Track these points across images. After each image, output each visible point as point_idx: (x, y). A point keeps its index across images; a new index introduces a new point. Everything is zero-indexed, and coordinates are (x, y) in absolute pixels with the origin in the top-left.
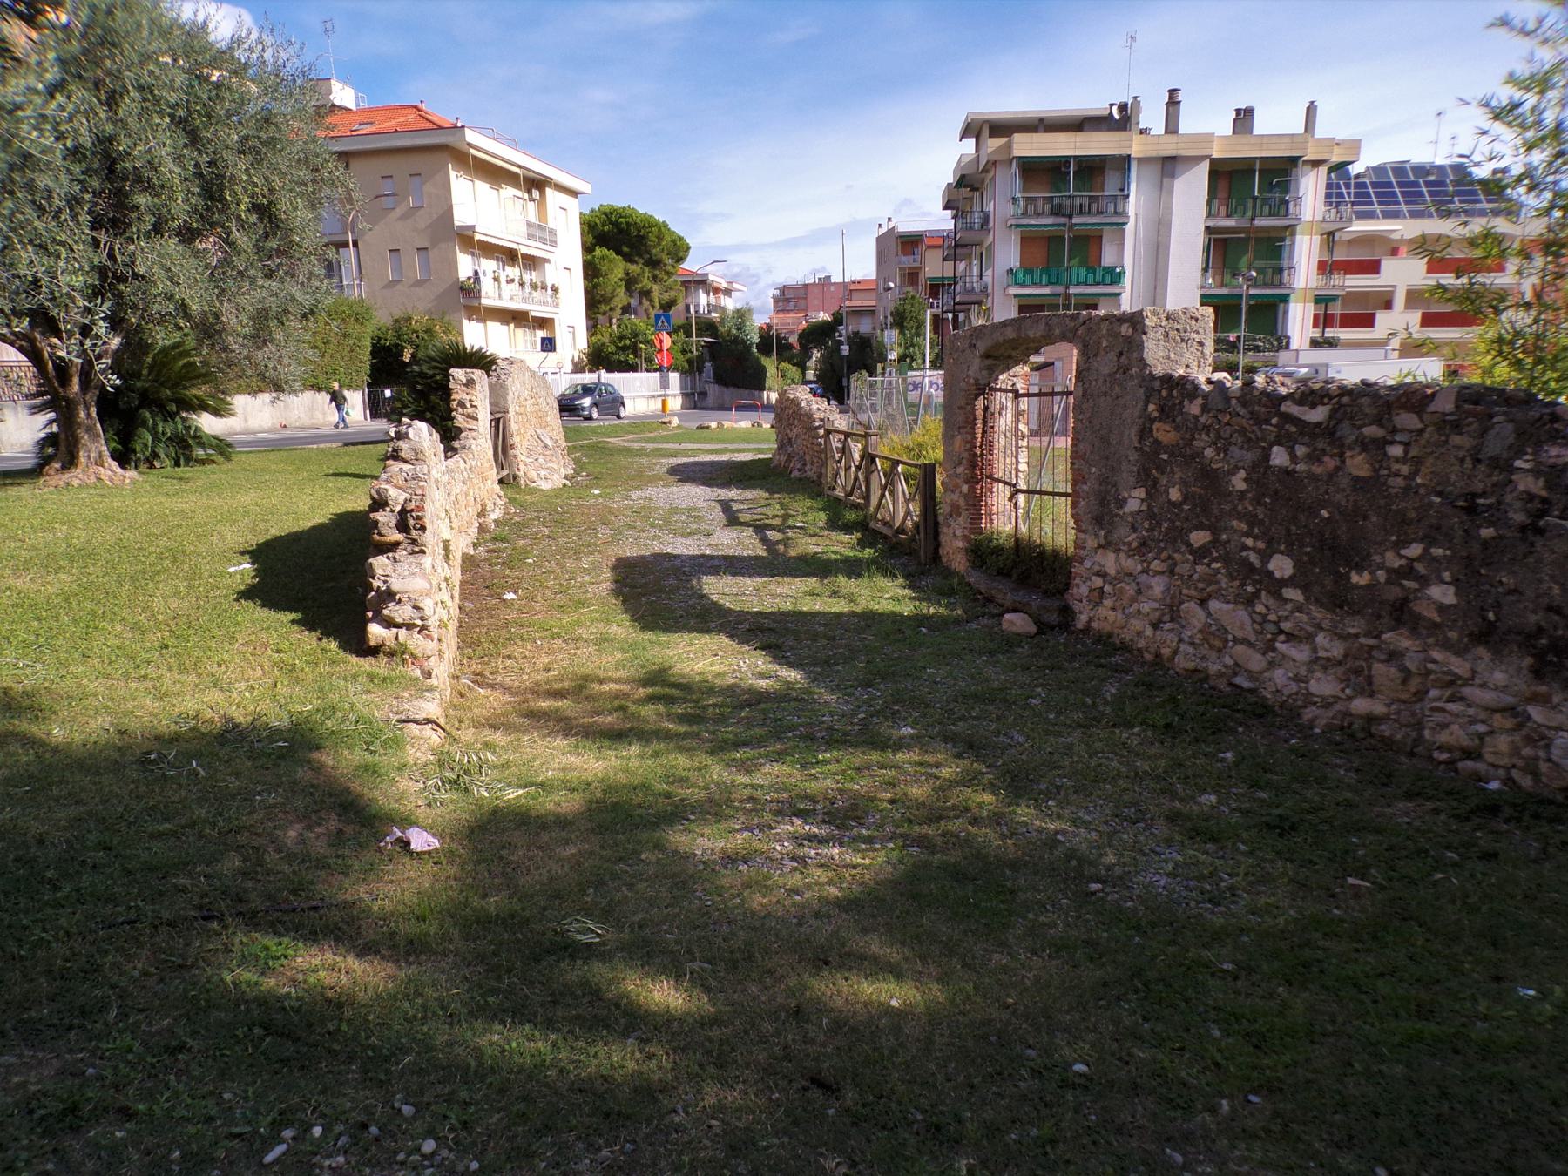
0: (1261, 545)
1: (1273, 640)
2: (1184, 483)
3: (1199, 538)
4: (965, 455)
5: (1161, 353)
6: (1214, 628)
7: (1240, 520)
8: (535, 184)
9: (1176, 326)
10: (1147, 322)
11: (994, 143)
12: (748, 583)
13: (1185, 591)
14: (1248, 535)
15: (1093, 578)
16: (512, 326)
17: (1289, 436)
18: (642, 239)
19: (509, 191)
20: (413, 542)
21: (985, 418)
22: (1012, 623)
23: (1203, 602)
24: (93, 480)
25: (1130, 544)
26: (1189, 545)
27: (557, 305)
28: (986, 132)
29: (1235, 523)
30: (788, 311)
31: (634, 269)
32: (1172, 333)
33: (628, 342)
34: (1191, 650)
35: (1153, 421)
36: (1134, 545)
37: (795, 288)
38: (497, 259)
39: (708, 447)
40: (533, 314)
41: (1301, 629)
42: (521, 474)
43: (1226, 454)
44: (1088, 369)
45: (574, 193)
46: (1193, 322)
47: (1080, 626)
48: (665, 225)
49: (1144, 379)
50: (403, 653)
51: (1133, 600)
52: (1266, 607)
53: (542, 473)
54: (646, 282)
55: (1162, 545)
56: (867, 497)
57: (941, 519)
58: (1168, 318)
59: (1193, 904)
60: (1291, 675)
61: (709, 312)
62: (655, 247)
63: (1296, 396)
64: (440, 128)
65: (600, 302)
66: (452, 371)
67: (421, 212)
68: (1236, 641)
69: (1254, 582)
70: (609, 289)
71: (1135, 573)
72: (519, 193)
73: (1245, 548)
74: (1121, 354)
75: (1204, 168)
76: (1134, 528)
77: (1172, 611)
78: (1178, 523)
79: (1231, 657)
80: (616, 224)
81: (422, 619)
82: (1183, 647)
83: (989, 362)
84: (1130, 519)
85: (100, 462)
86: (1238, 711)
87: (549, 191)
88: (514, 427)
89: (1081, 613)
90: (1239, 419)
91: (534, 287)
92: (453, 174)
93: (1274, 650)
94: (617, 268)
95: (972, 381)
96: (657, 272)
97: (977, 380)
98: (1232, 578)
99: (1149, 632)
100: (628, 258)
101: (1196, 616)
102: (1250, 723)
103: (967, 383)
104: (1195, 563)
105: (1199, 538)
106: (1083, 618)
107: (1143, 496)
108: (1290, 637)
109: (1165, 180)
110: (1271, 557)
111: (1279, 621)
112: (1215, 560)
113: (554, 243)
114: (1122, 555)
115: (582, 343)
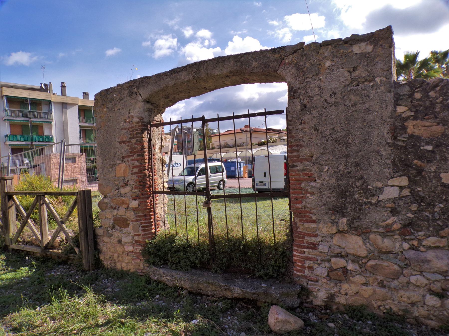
83: (149, 106)
84: (390, 205)
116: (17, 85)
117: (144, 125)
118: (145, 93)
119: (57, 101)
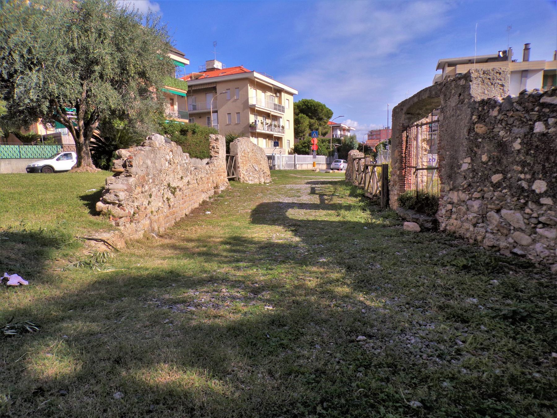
0: (528, 176)
1: (535, 228)
2: (489, 151)
3: (496, 178)
4: (399, 158)
5: (480, 91)
6: (504, 223)
7: (517, 165)
8: (278, 91)
9: (488, 77)
10: (472, 75)
11: (448, 69)
12: (303, 211)
13: (489, 206)
14: (521, 172)
15: (448, 205)
16: (267, 139)
17: (545, 115)
18: (316, 110)
19: (269, 94)
20: (127, 171)
21: (407, 141)
22: (408, 226)
23: (498, 211)
24: (85, 170)
25: (463, 185)
26: (492, 182)
27: (284, 133)
28: (446, 65)
29: (515, 167)
30: (373, 139)
31: (312, 121)
32: (486, 81)
33: (306, 144)
34: (491, 236)
35: (474, 124)
36: (465, 186)
37: (376, 131)
38: (263, 117)
39: (324, 177)
40: (275, 135)
41: (551, 220)
42: (241, 177)
43: (510, 132)
44: (446, 106)
45: (291, 94)
46: (498, 75)
47: (441, 229)
48: (324, 106)
49: (470, 104)
50: (109, 215)
51: (465, 213)
52: (532, 210)
53: (251, 178)
54: (316, 126)
55: (478, 184)
56: (365, 183)
57: (390, 188)
58: (484, 74)
59: (425, 356)
60: (545, 246)
61: (341, 137)
62: (320, 113)
63: (549, 92)
64: (246, 72)
65: (300, 133)
66: (210, 135)
67: (238, 101)
68: (515, 229)
69: (525, 197)
70: (303, 128)
71: (466, 200)
72: (272, 94)
73: (520, 179)
74: (460, 95)
75: (540, 75)
76: (465, 178)
77: (483, 217)
78: (486, 172)
79: (513, 238)
80: (307, 106)
81: (119, 201)
82: (487, 235)
83: (408, 116)
84: (463, 174)
85: (89, 165)
86: (513, 265)
87: (283, 94)
88: (240, 160)
89: (442, 223)
90: (517, 113)
91: (275, 126)
92: (249, 87)
93: (535, 233)
94: (306, 121)
95: (401, 125)
96: (321, 122)
97: (403, 124)
98: (513, 196)
99: (472, 229)
100: (311, 118)
101: (494, 217)
102: (518, 270)
103: (399, 126)
104: (494, 191)
105: (496, 178)
106: (443, 225)
107: (469, 161)
108: (545, 225)
109: (523, 79)
110: (533, 182)
111: (539, 217)
112: (505, 188)
113: (283, 111)
114: (460, 192)
115: (292, 146)
116: (479, 57)
117: (404, 128)
118: (405, 109)
119: (516, 70)
